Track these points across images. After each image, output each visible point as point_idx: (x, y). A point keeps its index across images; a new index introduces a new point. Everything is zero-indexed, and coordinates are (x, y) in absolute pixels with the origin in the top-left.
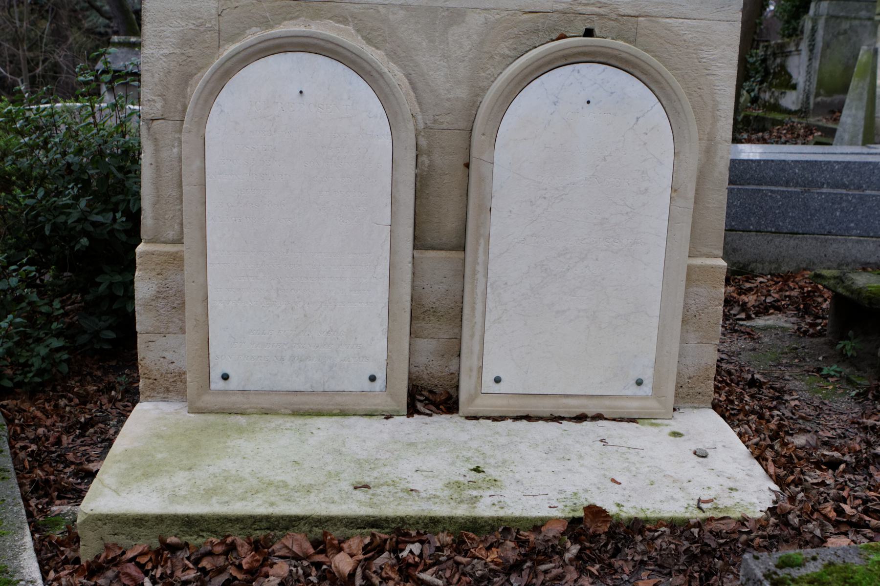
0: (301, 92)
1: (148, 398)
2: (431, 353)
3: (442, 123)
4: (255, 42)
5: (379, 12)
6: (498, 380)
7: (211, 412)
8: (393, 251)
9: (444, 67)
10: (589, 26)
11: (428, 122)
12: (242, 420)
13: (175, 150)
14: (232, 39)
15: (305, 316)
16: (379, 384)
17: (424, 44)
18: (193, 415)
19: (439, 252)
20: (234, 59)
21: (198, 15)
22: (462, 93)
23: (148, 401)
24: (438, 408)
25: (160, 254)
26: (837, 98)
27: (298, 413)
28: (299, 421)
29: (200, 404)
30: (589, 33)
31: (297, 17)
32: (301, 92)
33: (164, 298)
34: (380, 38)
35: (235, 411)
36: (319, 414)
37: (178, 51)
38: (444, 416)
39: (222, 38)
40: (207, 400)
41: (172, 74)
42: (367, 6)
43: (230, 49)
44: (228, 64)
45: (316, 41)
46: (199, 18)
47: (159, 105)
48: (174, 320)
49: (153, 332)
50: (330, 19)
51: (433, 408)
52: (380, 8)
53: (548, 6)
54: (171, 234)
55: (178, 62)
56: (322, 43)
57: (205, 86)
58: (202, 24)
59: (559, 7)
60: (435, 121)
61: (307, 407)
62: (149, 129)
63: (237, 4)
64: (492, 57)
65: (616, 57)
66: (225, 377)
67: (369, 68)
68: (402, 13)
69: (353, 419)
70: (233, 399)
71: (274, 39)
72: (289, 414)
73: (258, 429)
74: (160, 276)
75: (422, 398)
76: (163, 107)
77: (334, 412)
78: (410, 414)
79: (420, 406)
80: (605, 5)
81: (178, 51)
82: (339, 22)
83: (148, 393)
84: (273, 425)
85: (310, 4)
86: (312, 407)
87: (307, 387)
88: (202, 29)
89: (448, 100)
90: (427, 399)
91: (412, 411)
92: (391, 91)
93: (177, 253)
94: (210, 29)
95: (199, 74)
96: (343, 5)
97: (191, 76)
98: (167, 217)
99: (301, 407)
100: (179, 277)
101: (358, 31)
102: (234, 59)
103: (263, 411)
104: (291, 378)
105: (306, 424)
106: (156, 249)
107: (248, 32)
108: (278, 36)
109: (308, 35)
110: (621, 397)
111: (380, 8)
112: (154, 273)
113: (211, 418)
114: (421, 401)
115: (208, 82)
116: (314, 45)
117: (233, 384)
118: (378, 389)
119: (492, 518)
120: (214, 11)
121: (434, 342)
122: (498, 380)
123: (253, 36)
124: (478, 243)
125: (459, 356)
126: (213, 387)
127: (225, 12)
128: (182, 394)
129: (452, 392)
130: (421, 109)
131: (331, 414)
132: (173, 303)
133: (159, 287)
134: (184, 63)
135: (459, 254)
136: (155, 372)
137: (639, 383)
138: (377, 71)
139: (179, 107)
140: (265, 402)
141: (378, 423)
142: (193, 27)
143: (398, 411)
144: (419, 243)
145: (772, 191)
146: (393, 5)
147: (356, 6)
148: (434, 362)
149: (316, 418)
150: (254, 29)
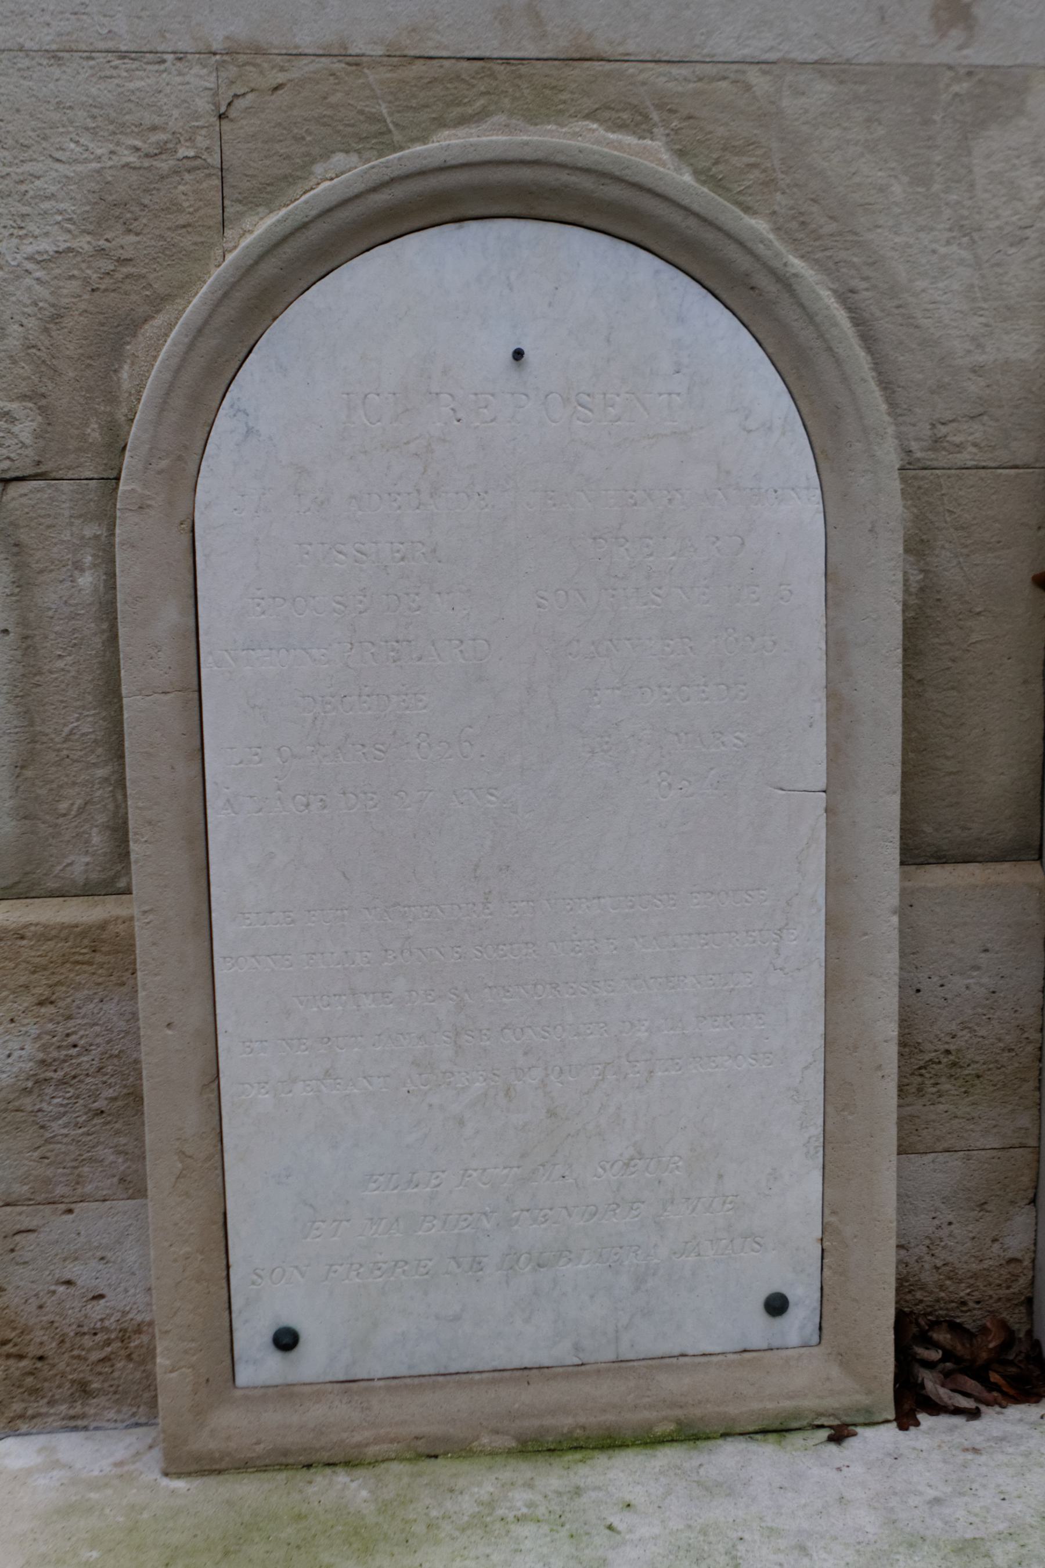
0: (518, 354)
2: (945, 1200)
3: (960, 447)
4: (360, 187)
5: (748, 88)
7: (245, 1466)
8: (837, 880)
9: (962, 262)
11: (914, 446)
12: (352, 1489)
13: (86, 580)
14: (265, 195)
15: (552, 1114)
17: (897, 189)
18: (180, 1484)
19: (962, 869)
20: (288, 250)
21: (149, 118)
23: (16, 1433)
24: (991, 1387)
25: (45, 934)
27: (542, 1445)
28: (553, 1478)
29: (203, 1442)
32: (518, 354)
33: (62, 1082)
34: (755, 174)
35: (325, 1456)
36: (610, 1441)
37: (84, 243)
38: (1015, 1411)
39: (232, 193)
40: (231, 1426)
41: (68, 322)
42: (709, 70)
43: (260, 227)
44: (268, 269)
45: (564, 177)
46: (154, 128)
48: (100, 1152)
49: (28, 1201)
50: (590, 116)
51: (971, 1385)
52: (753, 76)
54: (79, 865)
55: (86, 281)
56: (587, 183)
57: (191, 347)
58: (163, 150)
61: (566, 1422)
63: (281, 77)
66: (286, 1340)
67: (744, 263)
68: (823, 89)
69: (728, 1456)
70: (317, 1413)
71: (422, 173)
72: (510, 1452)
73: (419, 1528)
74: (48, 1010)
75: (935, 1355)
76: (37, 436)
77: (659, 1430)
78: (905, 1420)
79: (932, 1384)
81: (84, 243)
82: (621, 126)
83: (17, 1407)
84: (467, 1505)
85: (523, 69)
86: (582, 1420)
87: (562, 1353)
88: (164, 165)
89: (977, 370)
90: (948, 1355)
91: (910, 1404)
92: (821, 336)
93: (103, 926)
94: (193, 165)
95: (159, 320)
96: (631, 69)
97: (134, 325)
98: (63, 806)
99: (549, 1421)
100: (111, 1008)
101: (681, 154)
102: (288, 250)
103: (422, 1446)
104: (510, 1327)
105: (578, 1491)
106: (32, 918)
107: (318, 169)
108: (436, 162)
109: (540, 155)
111: (753, 76)
112: (26, 1001)
113: (249, 1491)
114: (929, 1365)
115: (200, 331)
116: (557, 193)
117: (312, 1362)
118: (793, 1338)
120: (202, 104)
121: (955, 1161)
123: (339, 176)
126: (245, 1375)
127: (241, 104)
128: (139, 1401)
129: (1015, 1319)
130: (892, 404)
131: (649, 1440)
132: (95, 1096)
133: (44, 1048)
134: (107, 282)
136: (39, 1335)
138: (773, 272)
139: (94, 432)
140: (423, 1415)
141: (809, 1461)
142: (133, 159)
143: (868, 1411)
146: (794, 64)
147: (675, 70)
148: (955, 1228)
149: (601, 1460)
150: (339, 159)
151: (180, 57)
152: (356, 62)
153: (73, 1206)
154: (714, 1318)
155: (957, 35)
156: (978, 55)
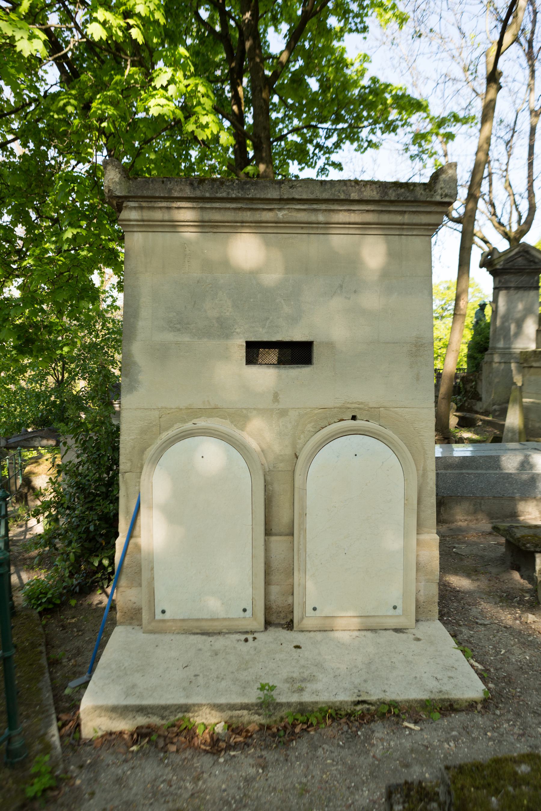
1: (122, 624)
6: (315, 609)
10: (354, 414)
13: (137, 488)
16: (249, 613)
18: (145, 635)
22: (288, 451)
26: (504, 405)
30: (354, 418)
31: (200, 417)
37: (139, 437)
39: (162, 429)
43: (164, 436)
47: (129, 465)
53: (331, 405)
59: (338, 405)
60: (274, 467)
62: (123, 478)
64: (303, 432)
65: (368, 431)
80: (362, 403)
110: (386, 616)
116: (209, 433)
117: (167, 616)
119: (312, 703)
120: (157, 416)
121: (278, 587)
122: (395, 608)
124: (300, 534)
125: (293, 594)
135: (290, 538)
137: (315, 609)
139: (139, 465)
144: (268, 532)
145: (468, 474)
151: (154, 409)
152: (181, 409)
153: (303, 685)
154: (214, 607)
155: (276, 404)
156: (280, 406)
